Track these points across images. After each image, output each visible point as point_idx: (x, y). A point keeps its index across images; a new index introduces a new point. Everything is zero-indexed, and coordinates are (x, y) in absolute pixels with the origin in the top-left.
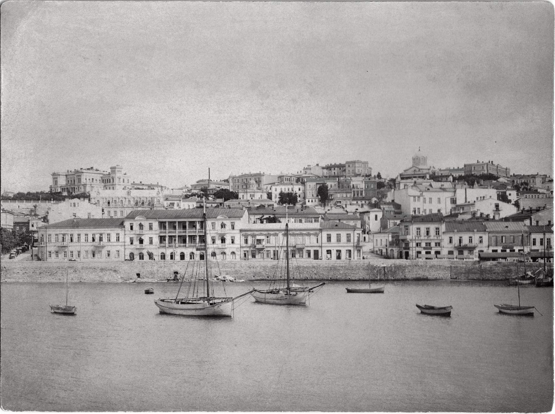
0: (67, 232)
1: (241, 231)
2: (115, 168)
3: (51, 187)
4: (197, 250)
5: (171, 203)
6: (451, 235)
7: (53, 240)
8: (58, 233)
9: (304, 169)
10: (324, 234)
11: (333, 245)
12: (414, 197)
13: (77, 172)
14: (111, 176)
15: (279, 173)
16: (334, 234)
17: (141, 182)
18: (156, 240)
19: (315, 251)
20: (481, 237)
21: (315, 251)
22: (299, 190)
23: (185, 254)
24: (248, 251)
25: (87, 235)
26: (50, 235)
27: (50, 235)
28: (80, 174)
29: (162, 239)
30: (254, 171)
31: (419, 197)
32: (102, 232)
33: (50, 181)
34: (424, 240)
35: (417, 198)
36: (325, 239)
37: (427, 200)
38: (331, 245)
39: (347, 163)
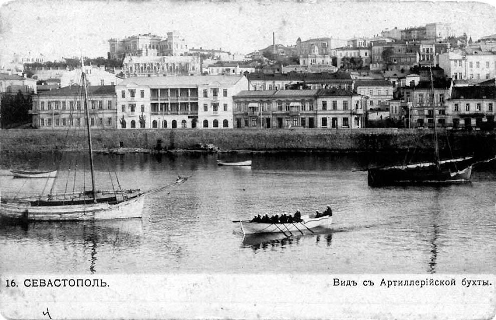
0: (96, 99)
1: (234, 97)
2: (171, 33)
3: (109, 54)
4: (189, 117)
5: (227, 70)
6: (457, 102)
7: (46, 107)
8: (51, 100)
9: (383, 32)
10: (320, 101)
11: (328, 112)
12: (456, 61)
13: (133, 38)
14: (168, 41)
15: (351, 38)
16: (329, 101)
17: (193, 48)
18: (148, 108)
19: (310, 118)
20: (468, 105)
21: (310, 118)
22: (366, 54)
23: (219, 121)
24: (241, 119)
25: (93, 102)
26: (43, 103)
27: (43, 103)
28: (135, 40)
29: (154, 106)
30: (321, 35)
31: (460, 61)
32: (94, 99)
33: (107, 49)
34: (427, 107)
35: (458, 62)
36: (320, 107)
37: (475, 65)
38: (326, 112)
39: (427, 25)
